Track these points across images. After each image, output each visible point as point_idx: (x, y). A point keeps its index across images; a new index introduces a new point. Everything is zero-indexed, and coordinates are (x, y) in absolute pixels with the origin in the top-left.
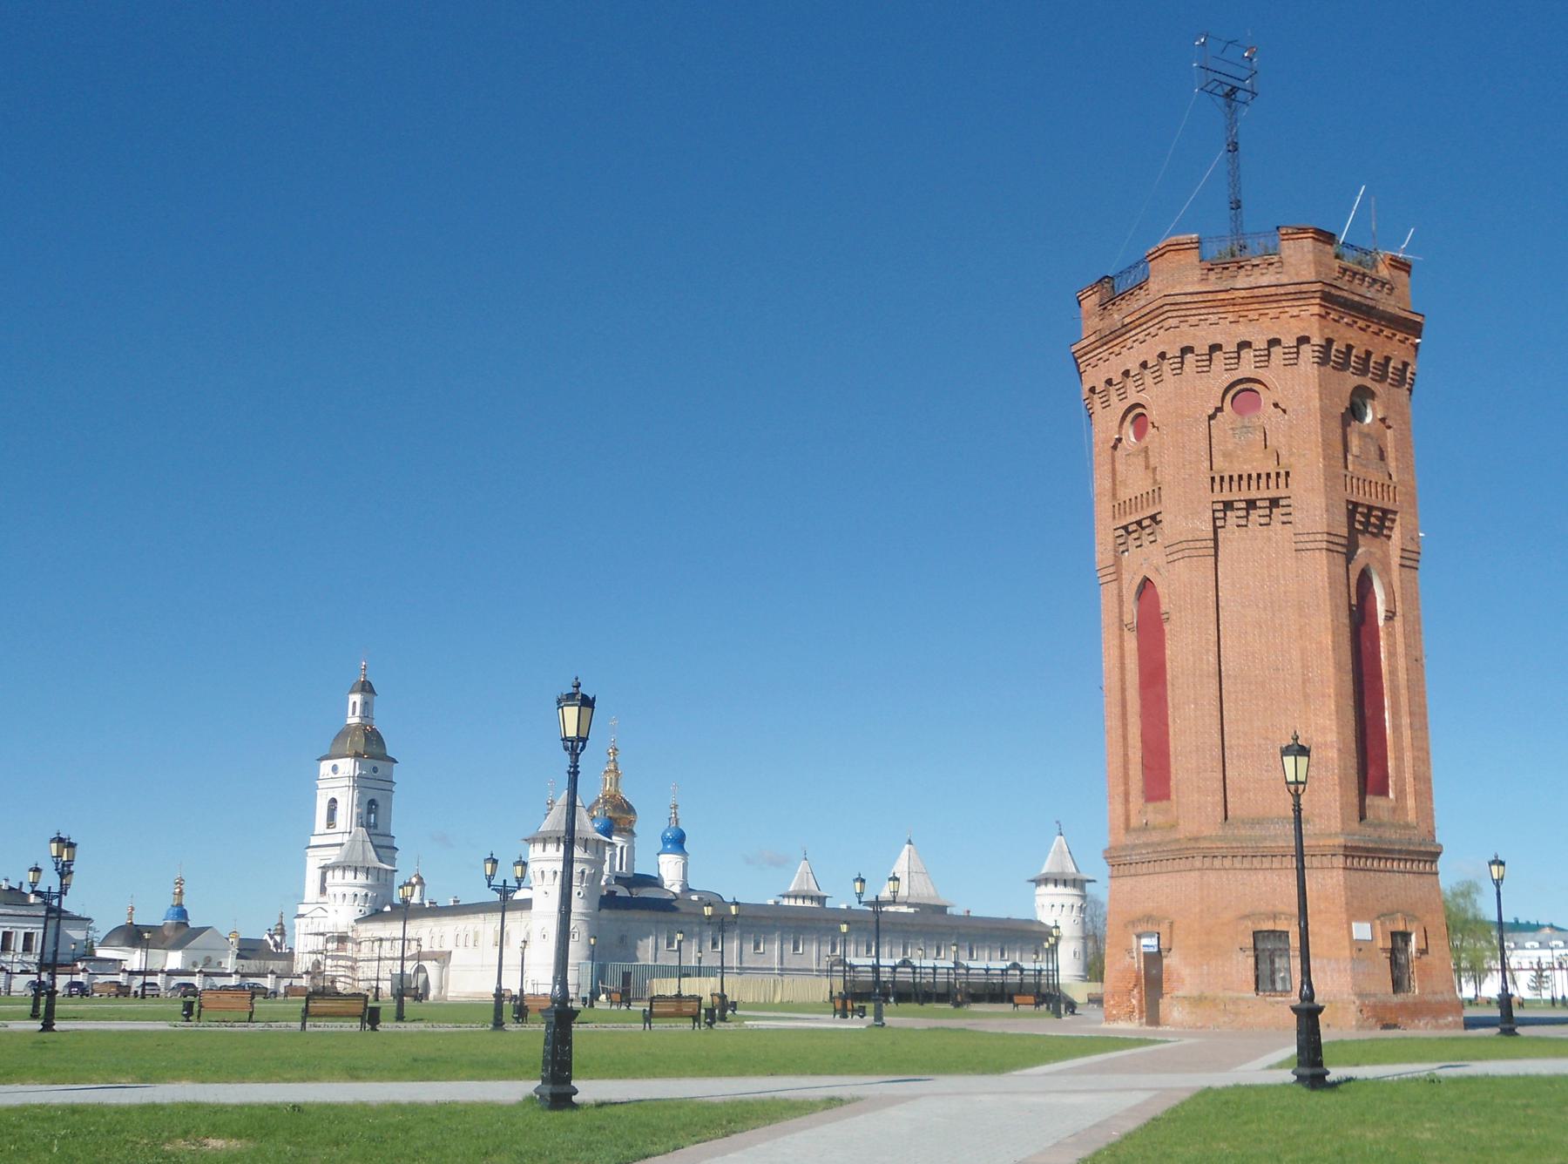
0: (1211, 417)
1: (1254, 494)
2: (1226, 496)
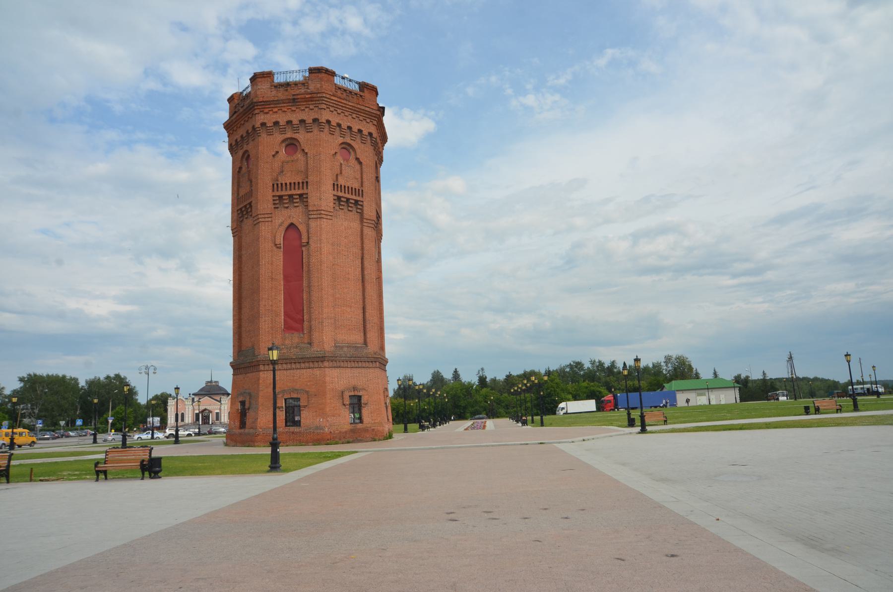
0: (274, 156)
1: (293, 192)
2: (340, 194)
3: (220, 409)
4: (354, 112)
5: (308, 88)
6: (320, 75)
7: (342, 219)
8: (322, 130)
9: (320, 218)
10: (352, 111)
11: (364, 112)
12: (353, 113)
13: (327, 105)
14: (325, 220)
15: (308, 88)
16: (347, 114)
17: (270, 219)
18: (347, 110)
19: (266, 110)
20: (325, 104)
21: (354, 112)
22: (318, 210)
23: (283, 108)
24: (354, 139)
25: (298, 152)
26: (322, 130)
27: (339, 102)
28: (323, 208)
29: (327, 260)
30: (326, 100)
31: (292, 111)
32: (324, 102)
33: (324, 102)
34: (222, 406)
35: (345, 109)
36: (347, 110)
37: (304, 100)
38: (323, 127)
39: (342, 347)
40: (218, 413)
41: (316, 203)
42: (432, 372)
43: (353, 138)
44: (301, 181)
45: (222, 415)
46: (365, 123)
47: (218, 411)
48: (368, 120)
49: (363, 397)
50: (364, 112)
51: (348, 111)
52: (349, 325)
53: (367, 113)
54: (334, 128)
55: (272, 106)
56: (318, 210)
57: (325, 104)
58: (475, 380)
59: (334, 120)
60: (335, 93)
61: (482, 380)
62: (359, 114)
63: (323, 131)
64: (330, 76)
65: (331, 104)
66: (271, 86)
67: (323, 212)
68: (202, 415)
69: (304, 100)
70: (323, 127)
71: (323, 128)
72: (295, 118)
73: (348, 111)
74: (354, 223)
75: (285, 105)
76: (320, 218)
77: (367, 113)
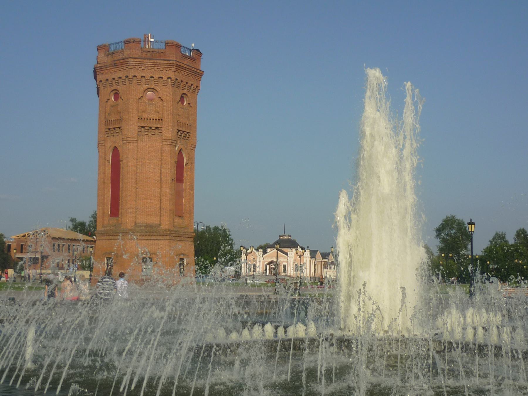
3: (287, 262)
4: (155, 66)
5: (123, 55)
6: (131, 45)
7: (147, 141)
8: (131, 83)
9: (128, 143)
10: (154, 66)
11: (163, 64)
12: (155, 67)
13: (134, 65)
14: (131, 144)
15: (123, 55)
16: (149, 68)
17: (103, 144)
18: (149, 65)
19: (102, 72)
20: (132, 65)
21: (155, 66)
22: (126, 138)
23: (110, 70)
24: (157, 84)
25: (119, 99)
26: (131, 83)
27: (142, 62)
28: (129, 136)
29: (131, 170)
30: (131, 62)
31: (115, 71)
32: (130, 64)
33: (130, 64)
34: (289, 259)
35: (148, 65)
36: (149, 65)
37: (119, 64)
38: (131, 81)
39: (140, 226)
40: (286, 265)
41: (126, 133)
42: (518, 229)
43: (155, 84)
44: (119, 119)
45: (289, 267)
46: (165, 72)
47: (285, 264)
48: (167, 69)
49: (153, 259)
50: (163, 64)
51: (150, 66)
52: (148, 212)
53: (166, 64)
54: (140, 80)
55: (104, 69)
56: (126, 138)
57: (132, 65)
58: (489, 243)
59: (139, 75)
60: (141, 55)
61: (491, 242)
62: (159, 66)
63: (131, 84)
64: (138, 44)
65: (136, 65)
66: (105, 55)
67: (129, 139)
68: (270, 267)
69: (119, 64)
70: (131, 81)
71: (132, 82)
72: (116, 76)
73: (150, 66)
74: (156, 143)
75: (111, 68)
76: (128, 143)
77: (166, 64)
